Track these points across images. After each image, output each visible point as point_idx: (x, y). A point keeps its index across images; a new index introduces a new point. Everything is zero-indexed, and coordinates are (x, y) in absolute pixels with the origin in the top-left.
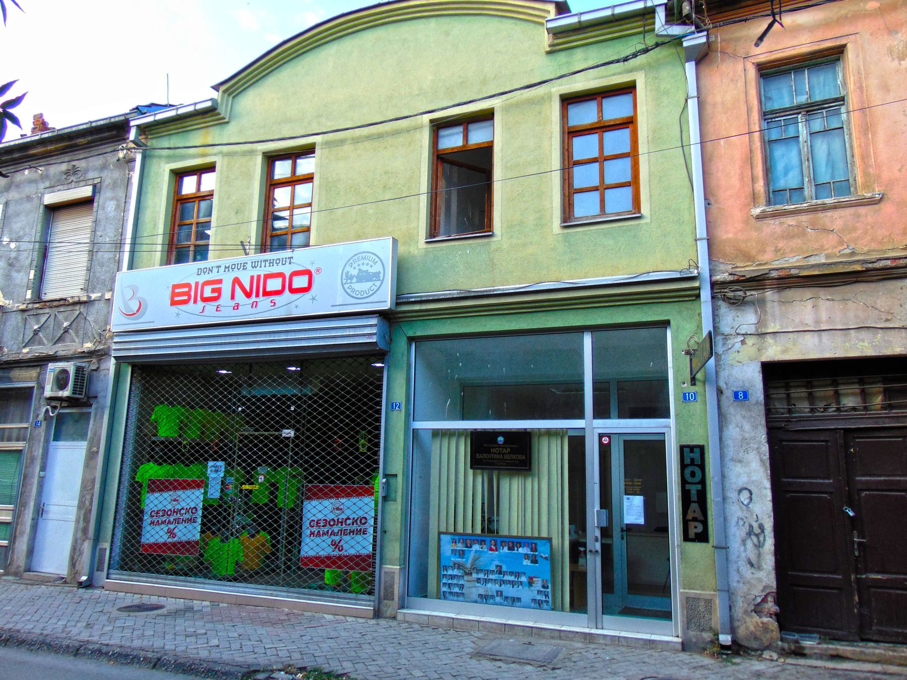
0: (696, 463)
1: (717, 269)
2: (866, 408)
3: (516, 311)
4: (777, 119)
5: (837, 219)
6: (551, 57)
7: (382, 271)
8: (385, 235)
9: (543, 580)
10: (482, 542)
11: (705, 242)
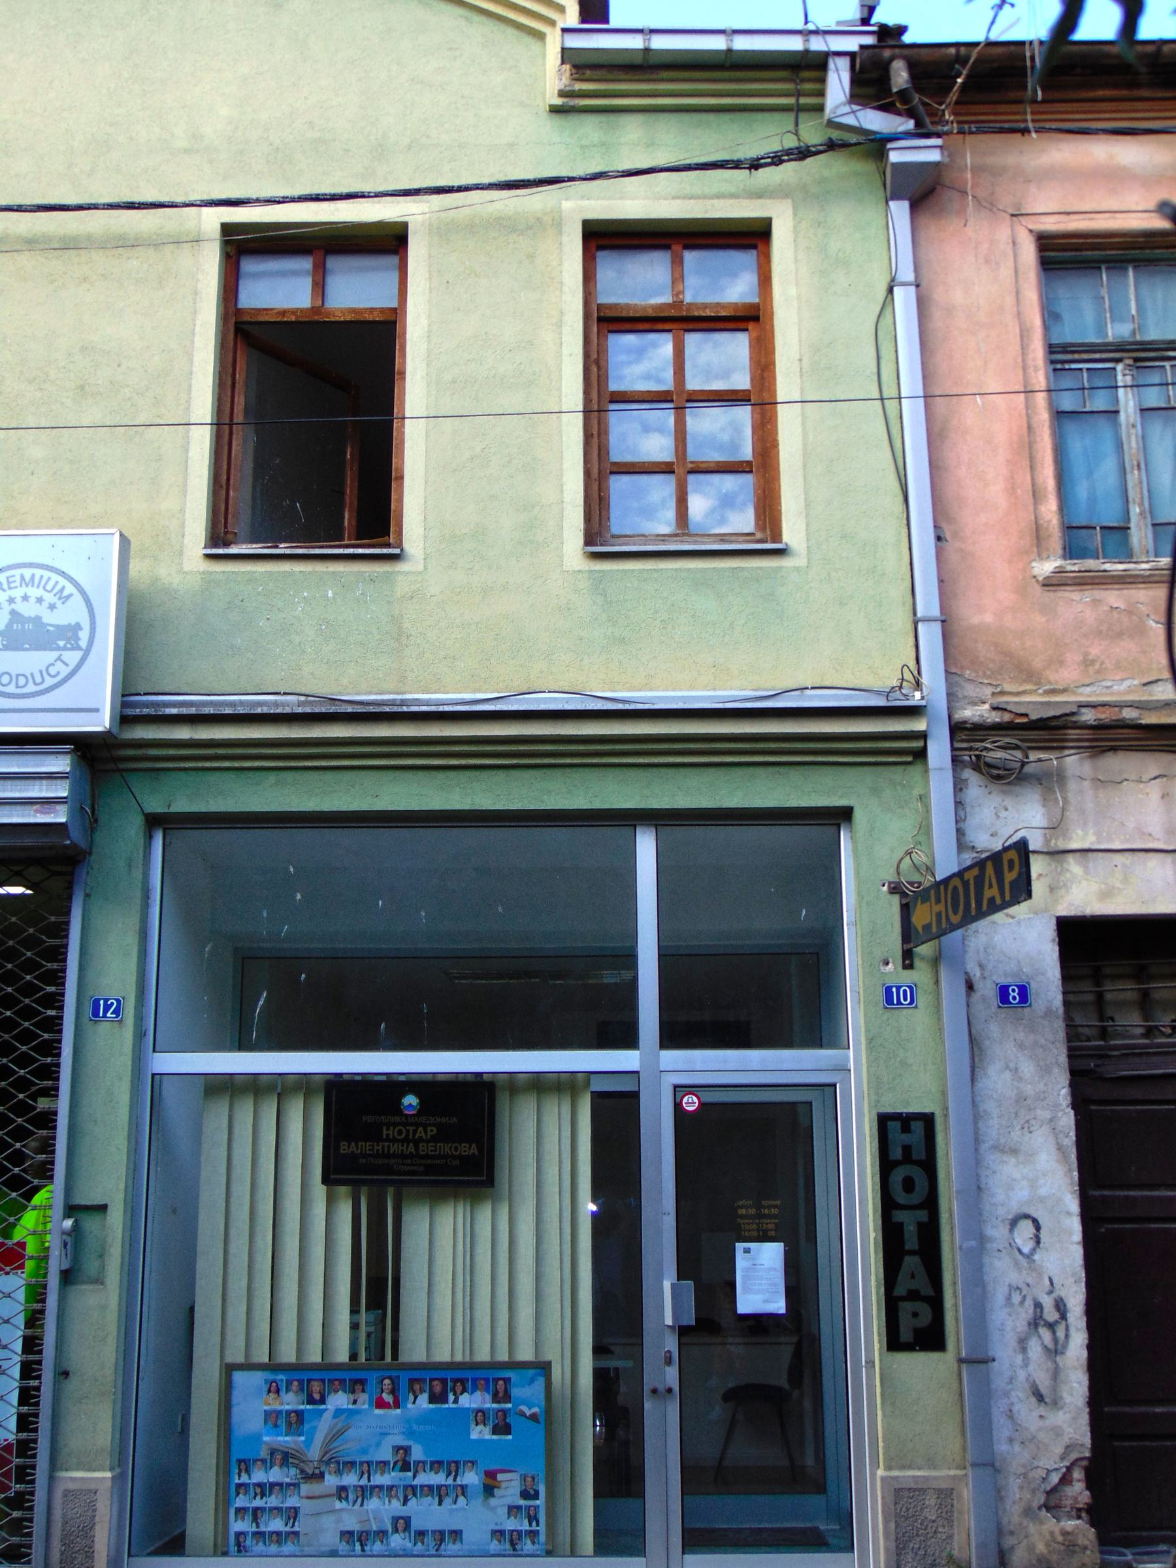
0: (915, 1157)
3: (463, 762)
4: (1074, 366)
6: (558, 120)
7: (86, 625)
8: (96, 521)
9: (524, 1478)
10: (355, 1385)
11: (937, 628)
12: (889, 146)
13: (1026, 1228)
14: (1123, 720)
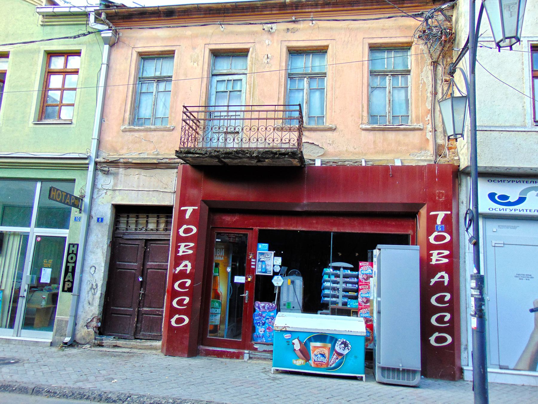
2: (157, 230)
4: (145, 82)
6: (42, 27)
12: (102, 32)
14: (129, 161)
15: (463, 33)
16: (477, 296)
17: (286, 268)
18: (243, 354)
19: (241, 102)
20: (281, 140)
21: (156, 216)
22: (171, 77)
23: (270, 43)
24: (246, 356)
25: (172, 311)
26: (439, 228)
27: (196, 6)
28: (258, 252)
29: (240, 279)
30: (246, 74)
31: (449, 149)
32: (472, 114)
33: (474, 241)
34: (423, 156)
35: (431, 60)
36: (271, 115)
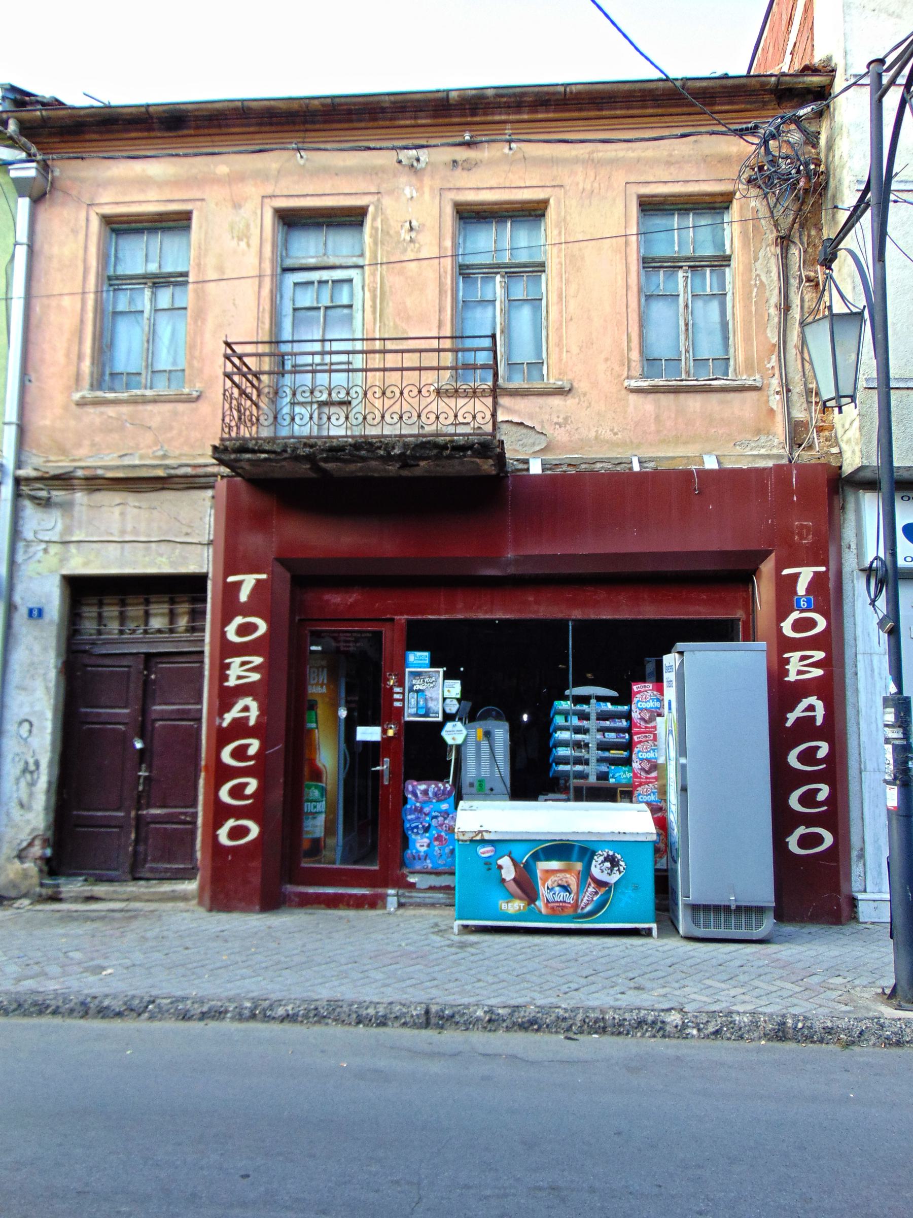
1: (29, 461)
4: (124, 287)
5: (156, 414)
12: (10, 167)
13: (26, 726)
15: (845, 172)
16: (897, 742)
17: (468, 705)
18: (383, 898)
19: (354, 332)
20: (456, 416)
21: (167, 599)
22: (185, 274)
23: (415, 194)
24: (392, 902)
25: (220, 813)
26: (803, 604)
27: (240, 104)
28: (407, 670)
29: (368, 734)
30: (362, 267)
31: (820, 430)
32: (880, 351)
33: (890, 624)
34: (763, 447)
35: (775, 234)
36: (430, 360)
